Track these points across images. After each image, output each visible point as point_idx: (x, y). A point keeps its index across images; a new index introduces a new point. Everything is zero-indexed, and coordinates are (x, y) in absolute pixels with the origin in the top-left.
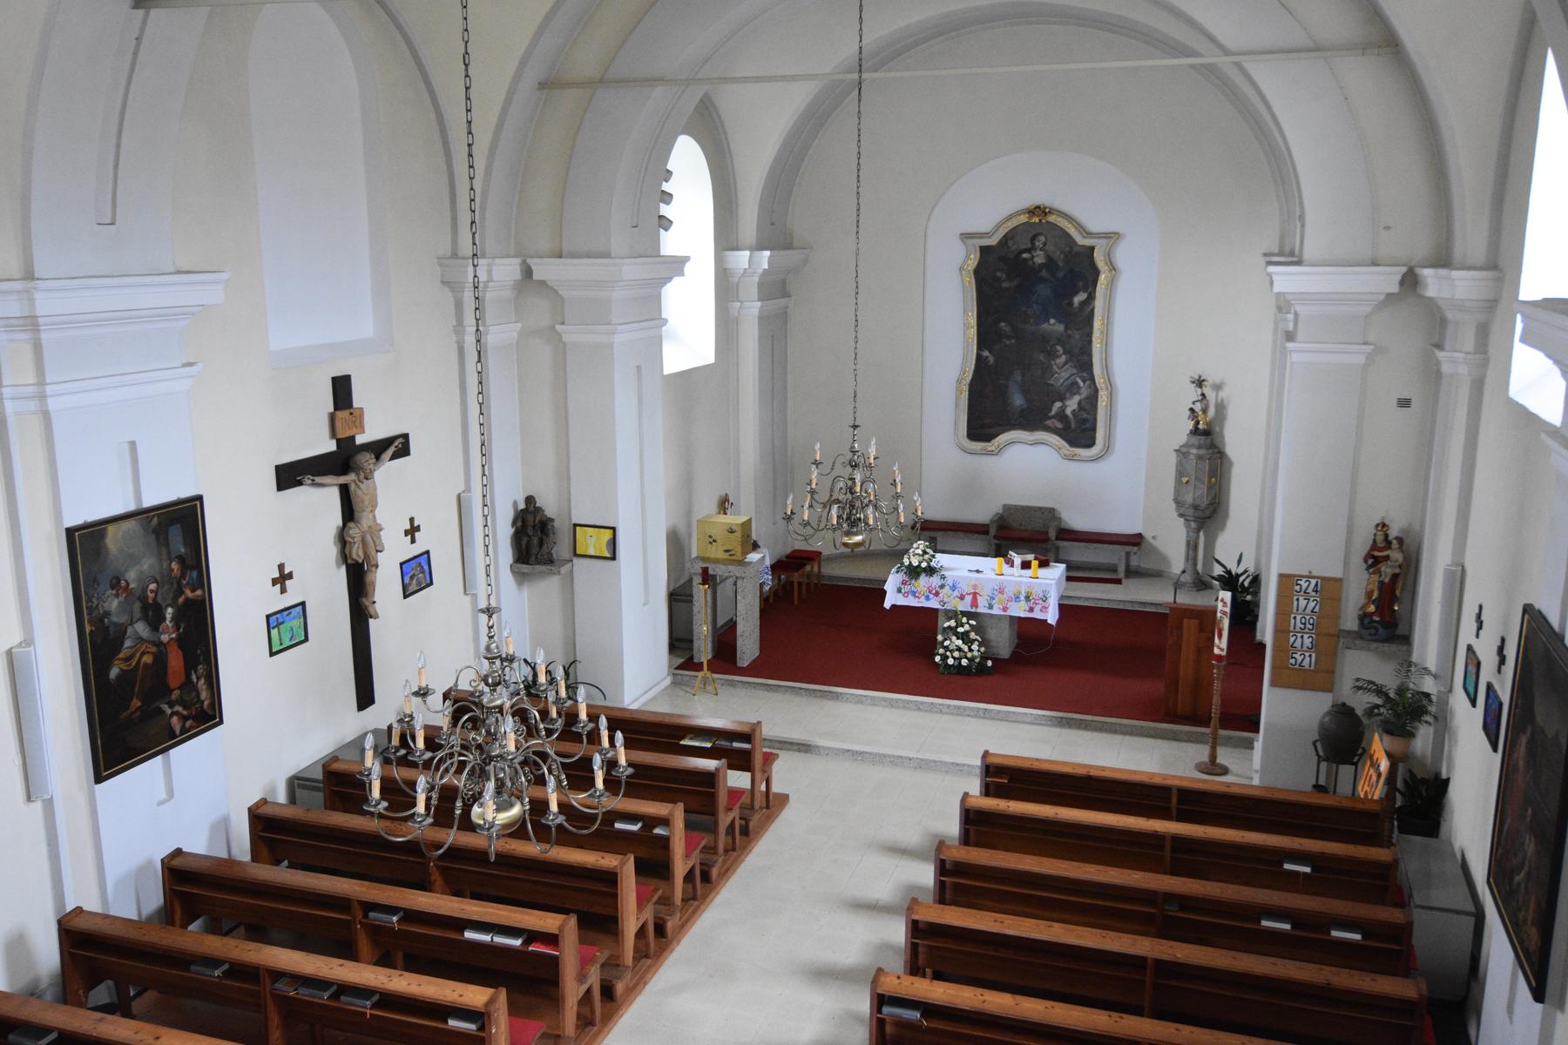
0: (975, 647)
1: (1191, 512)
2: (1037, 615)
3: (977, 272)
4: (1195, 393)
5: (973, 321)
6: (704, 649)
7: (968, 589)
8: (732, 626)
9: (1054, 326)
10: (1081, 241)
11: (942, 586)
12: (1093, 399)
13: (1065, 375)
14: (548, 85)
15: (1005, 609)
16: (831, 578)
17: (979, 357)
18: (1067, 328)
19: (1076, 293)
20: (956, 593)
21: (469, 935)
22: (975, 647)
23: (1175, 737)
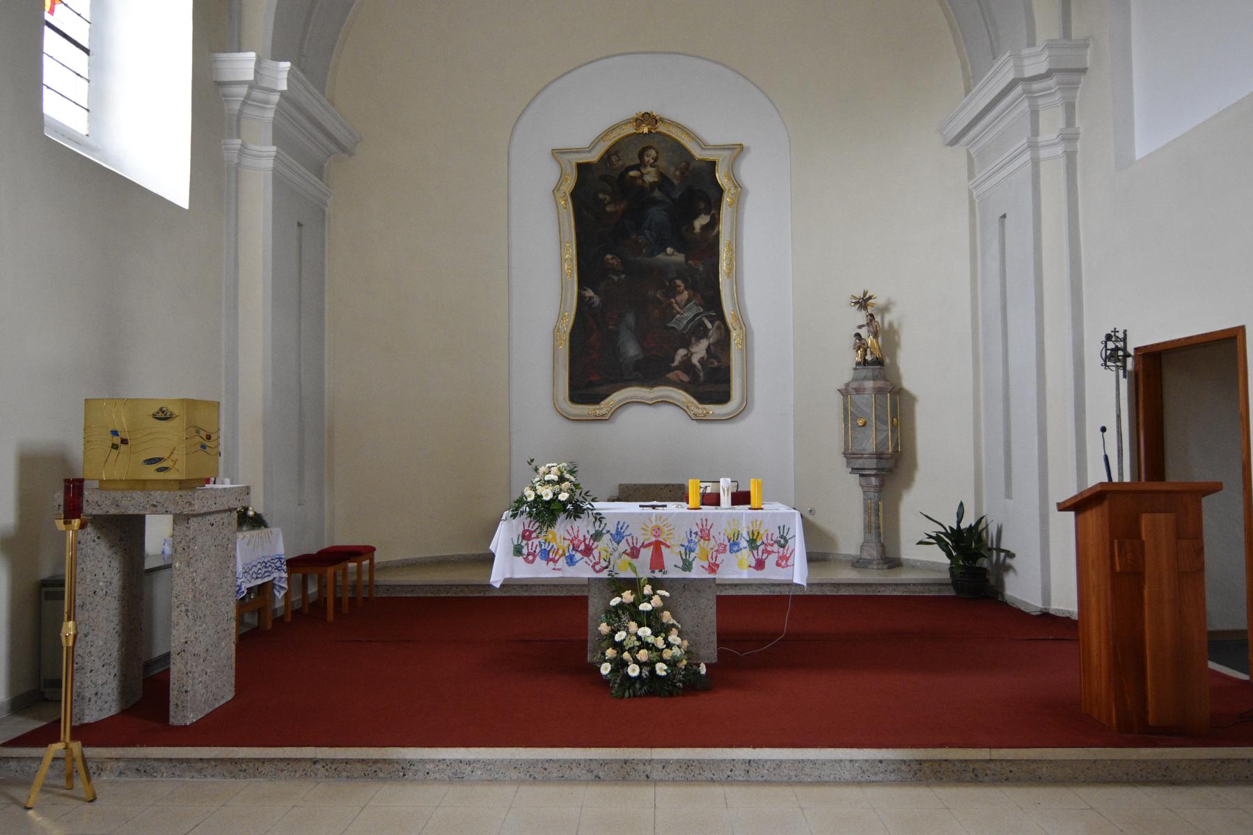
0: (674, 638)
1: (872, 463)
2: (772, 573)
3: (574, 195)
4: (861, 317)
6: (96, 689)
7: (643, 537)
9: (672, 256)
10: (698, 153)
11: (597, 536)
12: (724, 342)
13: (689, 315)
15: (713, 568)
16: (390, 587)
17: (581, 298)
18: (687, 259)
19: (696, 216)
20: (623, 546)
22: (674, 638)
23: (1166, 777)
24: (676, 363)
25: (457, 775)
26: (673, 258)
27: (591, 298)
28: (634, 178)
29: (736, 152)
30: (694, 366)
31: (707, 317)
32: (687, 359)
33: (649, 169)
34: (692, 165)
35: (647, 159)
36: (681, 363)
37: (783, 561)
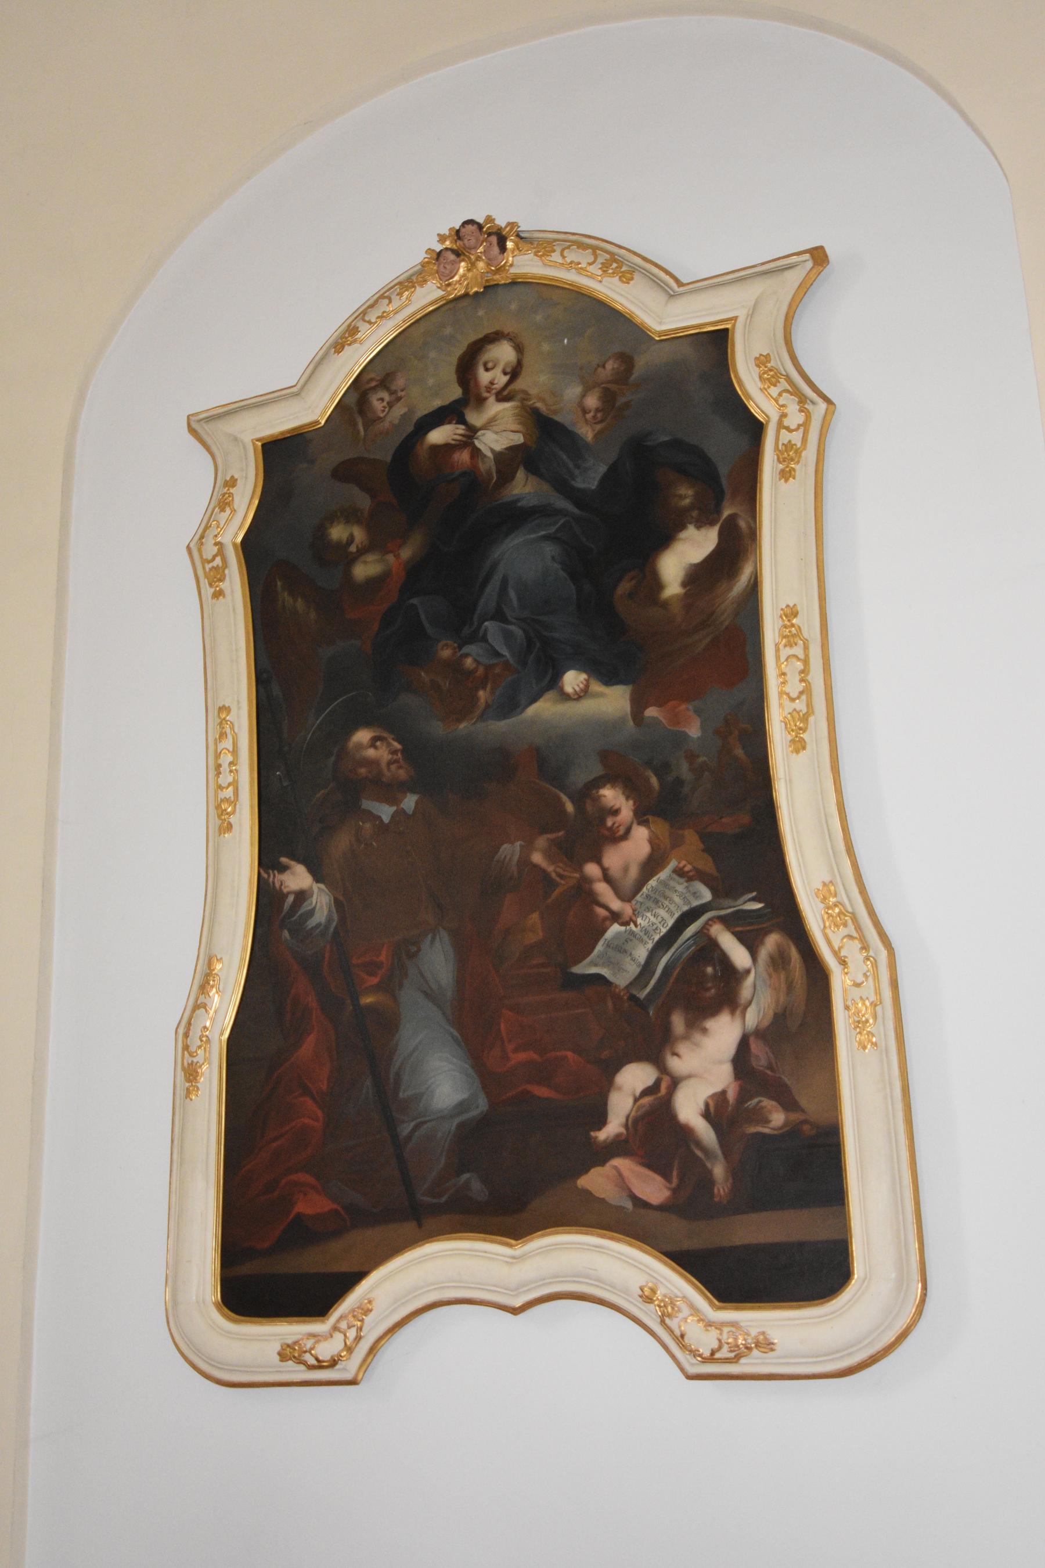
3: (252, 548)
8: (626, 277)
9: (587, 702)
10: (662, 316)
12: (805, 1025)
13: (657, 921)
17: (270, 906)
18: (638, 704)
19: (665, 539)
24: (613, 1127)
26: (587, 707)
27: (302, 896)
28: (447, 449)
29: (794, 278)
30: (685, 1133)
31: (728, 922)
33: (494, 408)
34: (642, 363)
35: (484, 377)
36: (633, 1124)
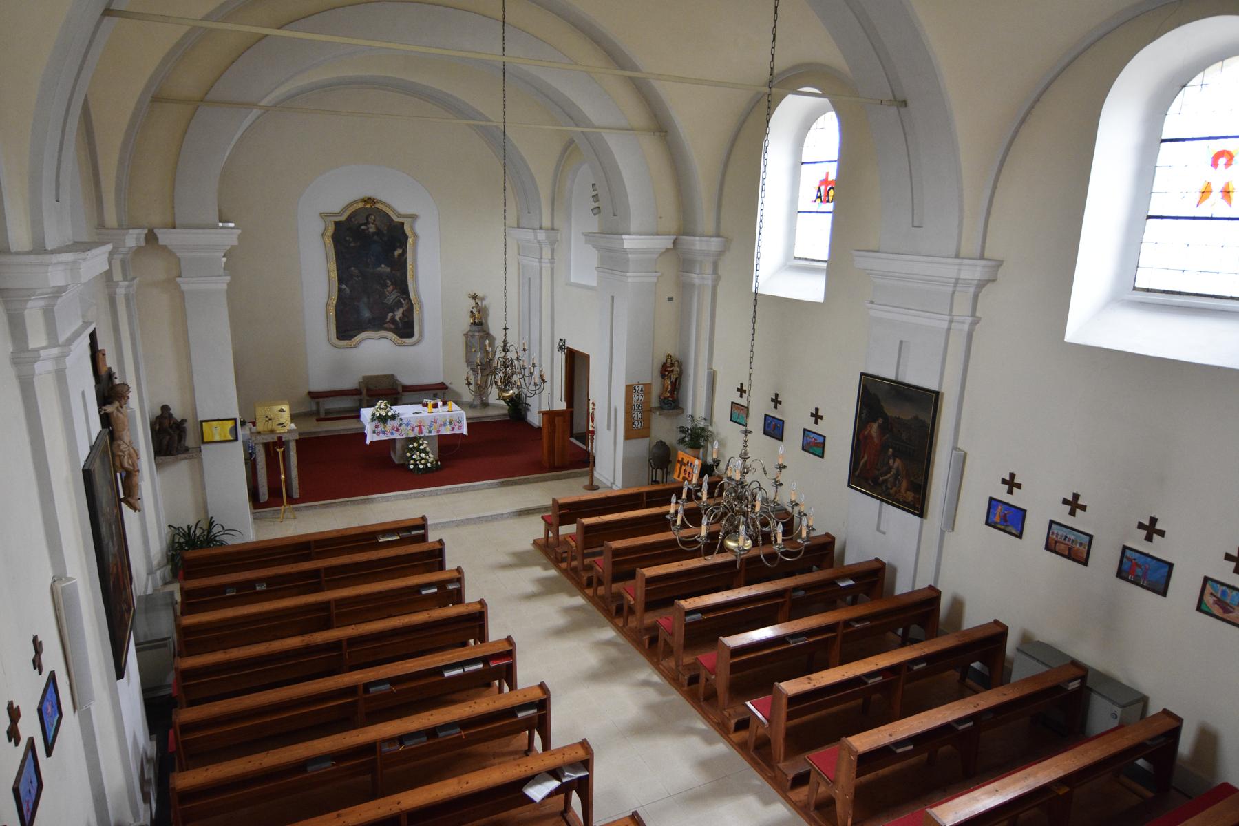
2: (457, 431)
5: (333, 266)
7: (415, 424)
9: (384, 269)
10: (396, 219)
12: (410, 310)
13: (393, 297)
14: (156, 99)
17: (340, 290)
21: (447, 674)
25: (387, 500)
32: (393, 318)
37: (460, 427)
